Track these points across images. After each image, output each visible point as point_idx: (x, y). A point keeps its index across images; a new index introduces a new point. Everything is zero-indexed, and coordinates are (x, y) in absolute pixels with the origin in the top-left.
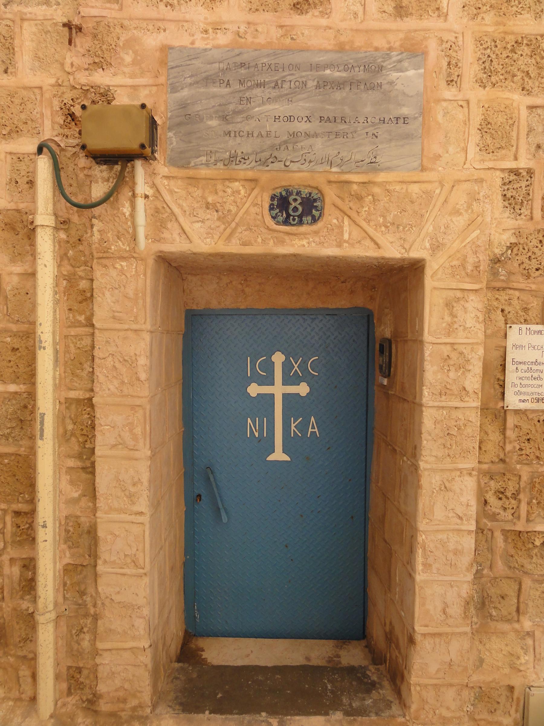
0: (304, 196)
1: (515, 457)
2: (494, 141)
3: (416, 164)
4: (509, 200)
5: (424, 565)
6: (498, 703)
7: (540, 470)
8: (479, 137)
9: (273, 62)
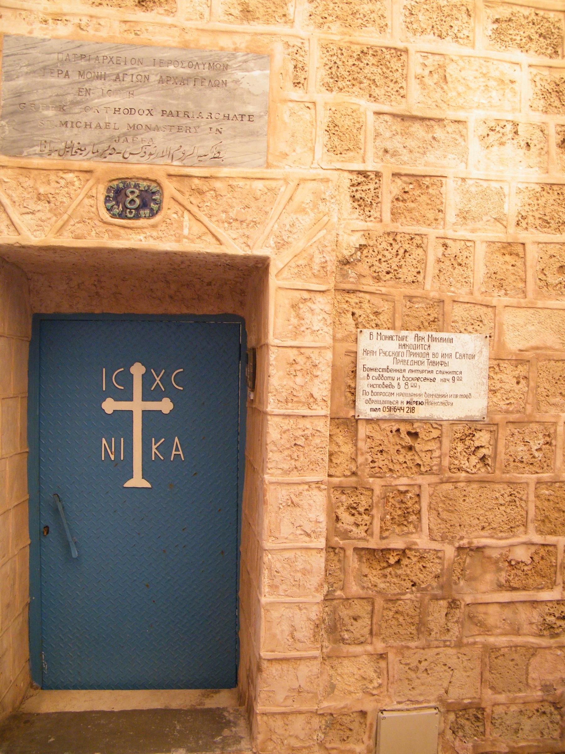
0: (142, 188)
1: (367, 470)
2: (342, 143)
3: (262, 160)
4: (359, 201)
5: (270, 586)
6: (351, 730)
7: (393, 484)
8: (327, 138)
9: (115, 55)
